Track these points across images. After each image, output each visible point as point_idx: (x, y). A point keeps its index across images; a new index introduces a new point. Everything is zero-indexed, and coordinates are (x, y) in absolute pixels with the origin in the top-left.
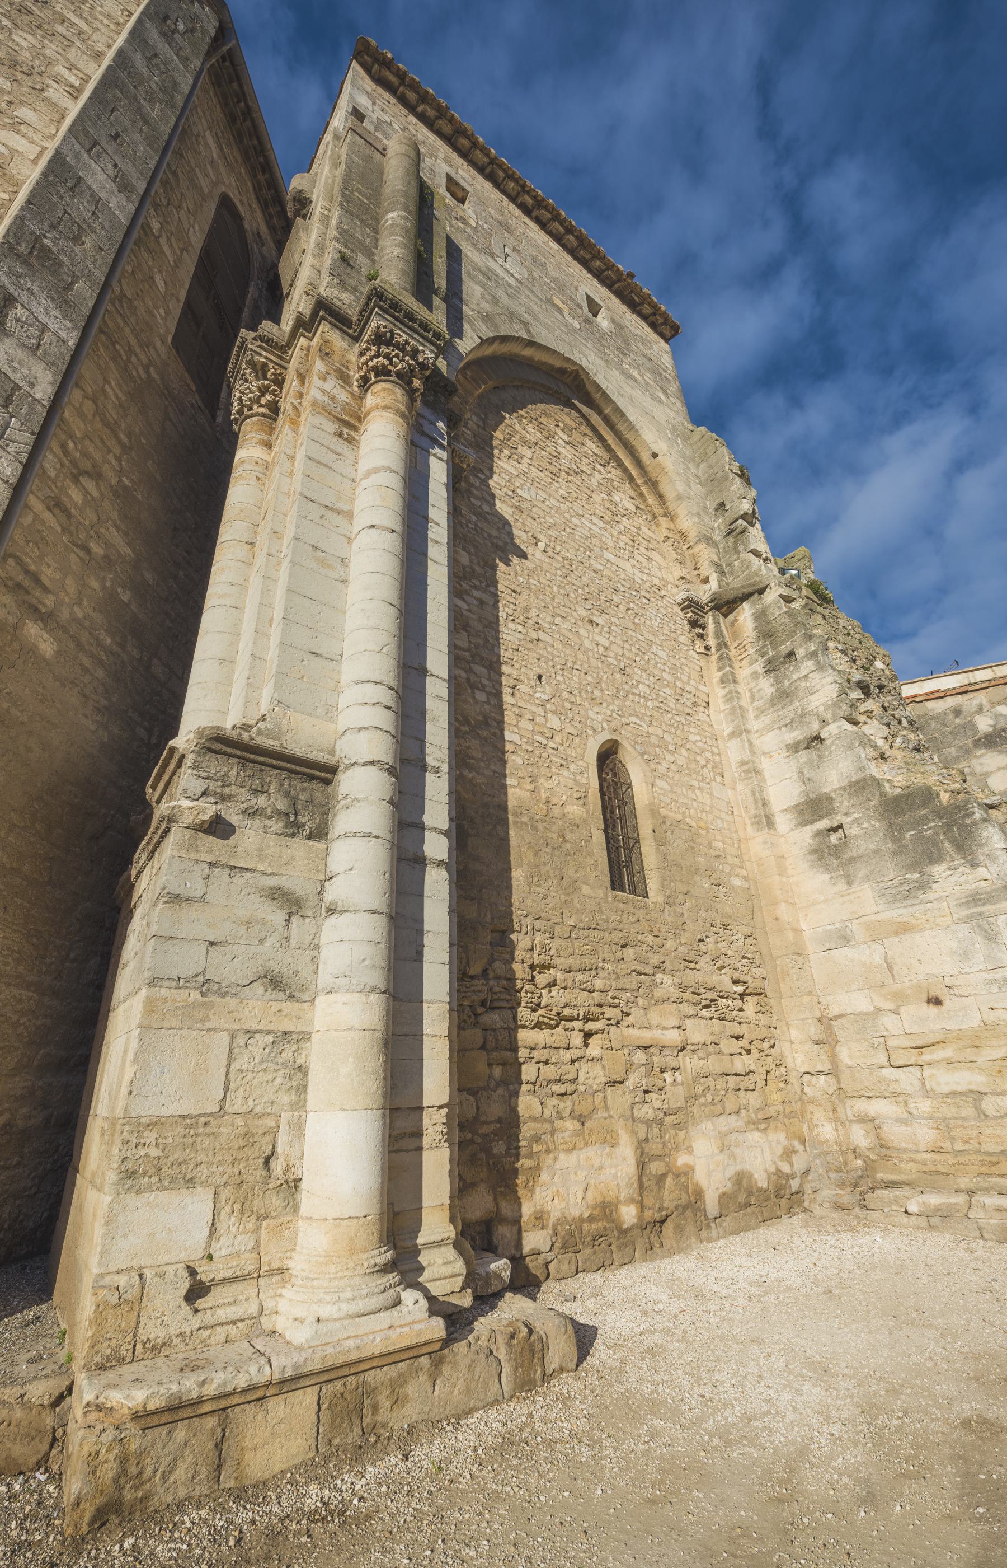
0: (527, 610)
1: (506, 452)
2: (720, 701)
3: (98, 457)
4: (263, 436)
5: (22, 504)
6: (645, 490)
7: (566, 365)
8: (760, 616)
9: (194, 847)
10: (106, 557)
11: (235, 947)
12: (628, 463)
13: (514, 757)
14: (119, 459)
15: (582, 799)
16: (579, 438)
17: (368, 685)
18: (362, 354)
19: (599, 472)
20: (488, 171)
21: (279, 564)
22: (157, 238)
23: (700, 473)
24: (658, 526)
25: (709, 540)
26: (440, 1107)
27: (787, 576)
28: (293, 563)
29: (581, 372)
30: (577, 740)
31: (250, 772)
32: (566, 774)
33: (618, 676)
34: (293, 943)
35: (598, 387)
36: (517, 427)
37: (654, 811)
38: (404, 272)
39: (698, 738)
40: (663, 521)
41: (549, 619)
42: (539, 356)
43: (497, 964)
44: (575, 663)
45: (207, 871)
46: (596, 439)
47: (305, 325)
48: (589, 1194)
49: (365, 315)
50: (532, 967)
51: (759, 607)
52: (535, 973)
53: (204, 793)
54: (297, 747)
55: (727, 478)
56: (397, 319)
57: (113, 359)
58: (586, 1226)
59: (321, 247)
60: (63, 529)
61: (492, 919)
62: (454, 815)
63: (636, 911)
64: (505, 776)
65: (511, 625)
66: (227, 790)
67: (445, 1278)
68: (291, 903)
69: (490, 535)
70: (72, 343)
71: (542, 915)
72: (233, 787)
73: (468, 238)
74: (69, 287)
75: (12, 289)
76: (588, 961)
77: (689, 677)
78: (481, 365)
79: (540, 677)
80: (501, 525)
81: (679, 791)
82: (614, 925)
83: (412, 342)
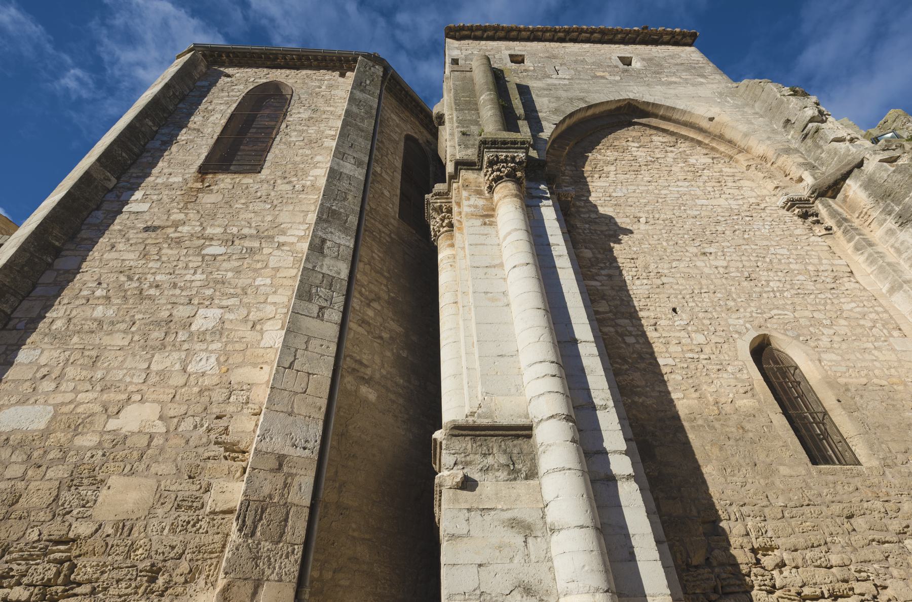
0: (646, 267)
1: (597, 176)
2: (864, 266)
3: (376, 289)
4: (449, 242)
5: (347, 329)
6: (714, 145)
7: (618, 105)
8: (869, 184)
9: (456, 500)
10: (391, 337)
11: (495, 566)
12: (692, 134)
13: (673, 376)
14: (386, 286)
15: (750, 391)
16: (648, 139)
17: (537, 365)
18: (485, 175)
19: (672, 152)
21: (470, 309)
22: (380, 175)
23: (757, 110)
24: (737, 162)
25: (788, 151)
27: (882, 142)
28: (476, 307)
30: (726, 346)
31: (479, 443)
32: (725, 375)
33: (745, 284)
34: (533, 557)
35: (648, 103)
36: (599, 157)
37: (831, 384)
38: (496, 121)
39: (853, 305)
40: (741, 157)
41: (666, 266)
42: (597, 110)
43: (716, 552)
44: (701, 288)
45: (467, 515)
46: (660, 134)
47: (455, 176)
49: (480, 155)
50: (754, 551)
51: (864, 177)
52: (759, 556)
53: (455, 464)
54: (503, 419)
55: (782, 102)
56: (497, 148)
57: (374, 240)
59: (452, 134)
60: (368, 332)
61: (699, 512)
62: (631, 435)
63: (851, 480)
64: (669, 393)
65: (638, 282)
66: (468, 458)
68: (524, 528)
69: (602, 232)
70: (352, 246)
71: (746, 501)
72: (471, 456)
73: (531, 78)
74: (346, 221)
75: (324, 236)
76: (814, 538)
77: (820, 258)
78: (561, 137)
79: (674, 310)
80: (607, 221)
81: (852, 357)
82: (829, 497)
83: (509, 154)
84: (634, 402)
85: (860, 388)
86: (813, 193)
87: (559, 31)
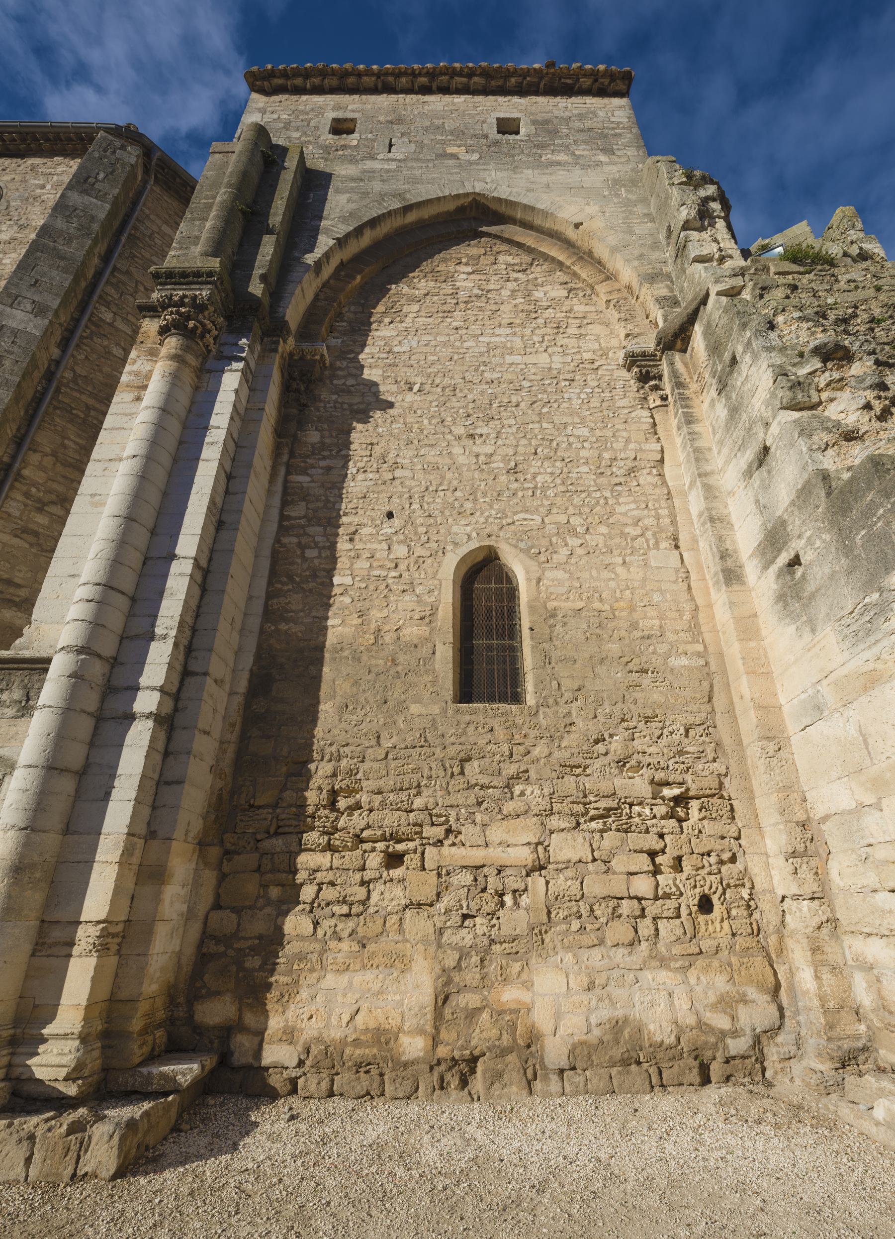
13: (342, 598)
20: (380, 86)
26: (98, 922)
29: (478, 198)
35: (499, 200)
42: (426, 213)
44: (440, 484)
46: (514, 250)
48: (359, 1018)
56: (175, 284)
58: (348, 1051)
60: (31, 545)
64: (327, 618)
67: (52, 1066)
84: (277, 630)
85: (570, 613)
86: (658, 345)
87: (420, 75)
